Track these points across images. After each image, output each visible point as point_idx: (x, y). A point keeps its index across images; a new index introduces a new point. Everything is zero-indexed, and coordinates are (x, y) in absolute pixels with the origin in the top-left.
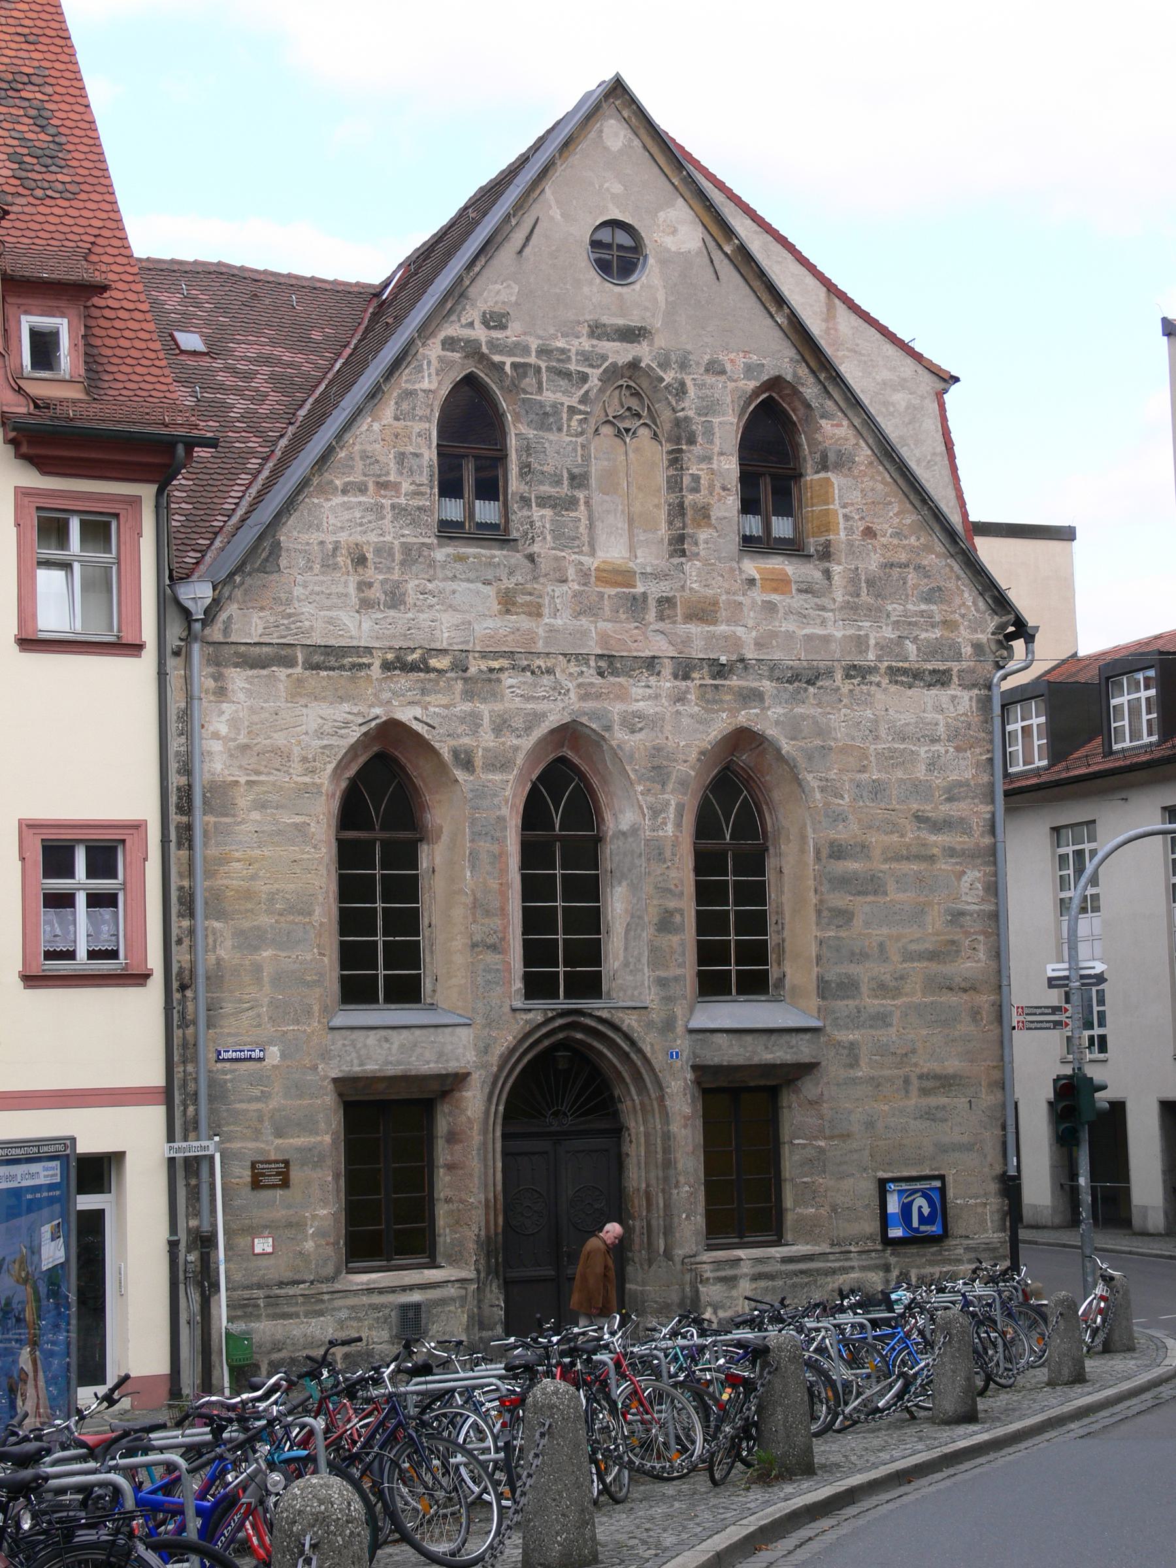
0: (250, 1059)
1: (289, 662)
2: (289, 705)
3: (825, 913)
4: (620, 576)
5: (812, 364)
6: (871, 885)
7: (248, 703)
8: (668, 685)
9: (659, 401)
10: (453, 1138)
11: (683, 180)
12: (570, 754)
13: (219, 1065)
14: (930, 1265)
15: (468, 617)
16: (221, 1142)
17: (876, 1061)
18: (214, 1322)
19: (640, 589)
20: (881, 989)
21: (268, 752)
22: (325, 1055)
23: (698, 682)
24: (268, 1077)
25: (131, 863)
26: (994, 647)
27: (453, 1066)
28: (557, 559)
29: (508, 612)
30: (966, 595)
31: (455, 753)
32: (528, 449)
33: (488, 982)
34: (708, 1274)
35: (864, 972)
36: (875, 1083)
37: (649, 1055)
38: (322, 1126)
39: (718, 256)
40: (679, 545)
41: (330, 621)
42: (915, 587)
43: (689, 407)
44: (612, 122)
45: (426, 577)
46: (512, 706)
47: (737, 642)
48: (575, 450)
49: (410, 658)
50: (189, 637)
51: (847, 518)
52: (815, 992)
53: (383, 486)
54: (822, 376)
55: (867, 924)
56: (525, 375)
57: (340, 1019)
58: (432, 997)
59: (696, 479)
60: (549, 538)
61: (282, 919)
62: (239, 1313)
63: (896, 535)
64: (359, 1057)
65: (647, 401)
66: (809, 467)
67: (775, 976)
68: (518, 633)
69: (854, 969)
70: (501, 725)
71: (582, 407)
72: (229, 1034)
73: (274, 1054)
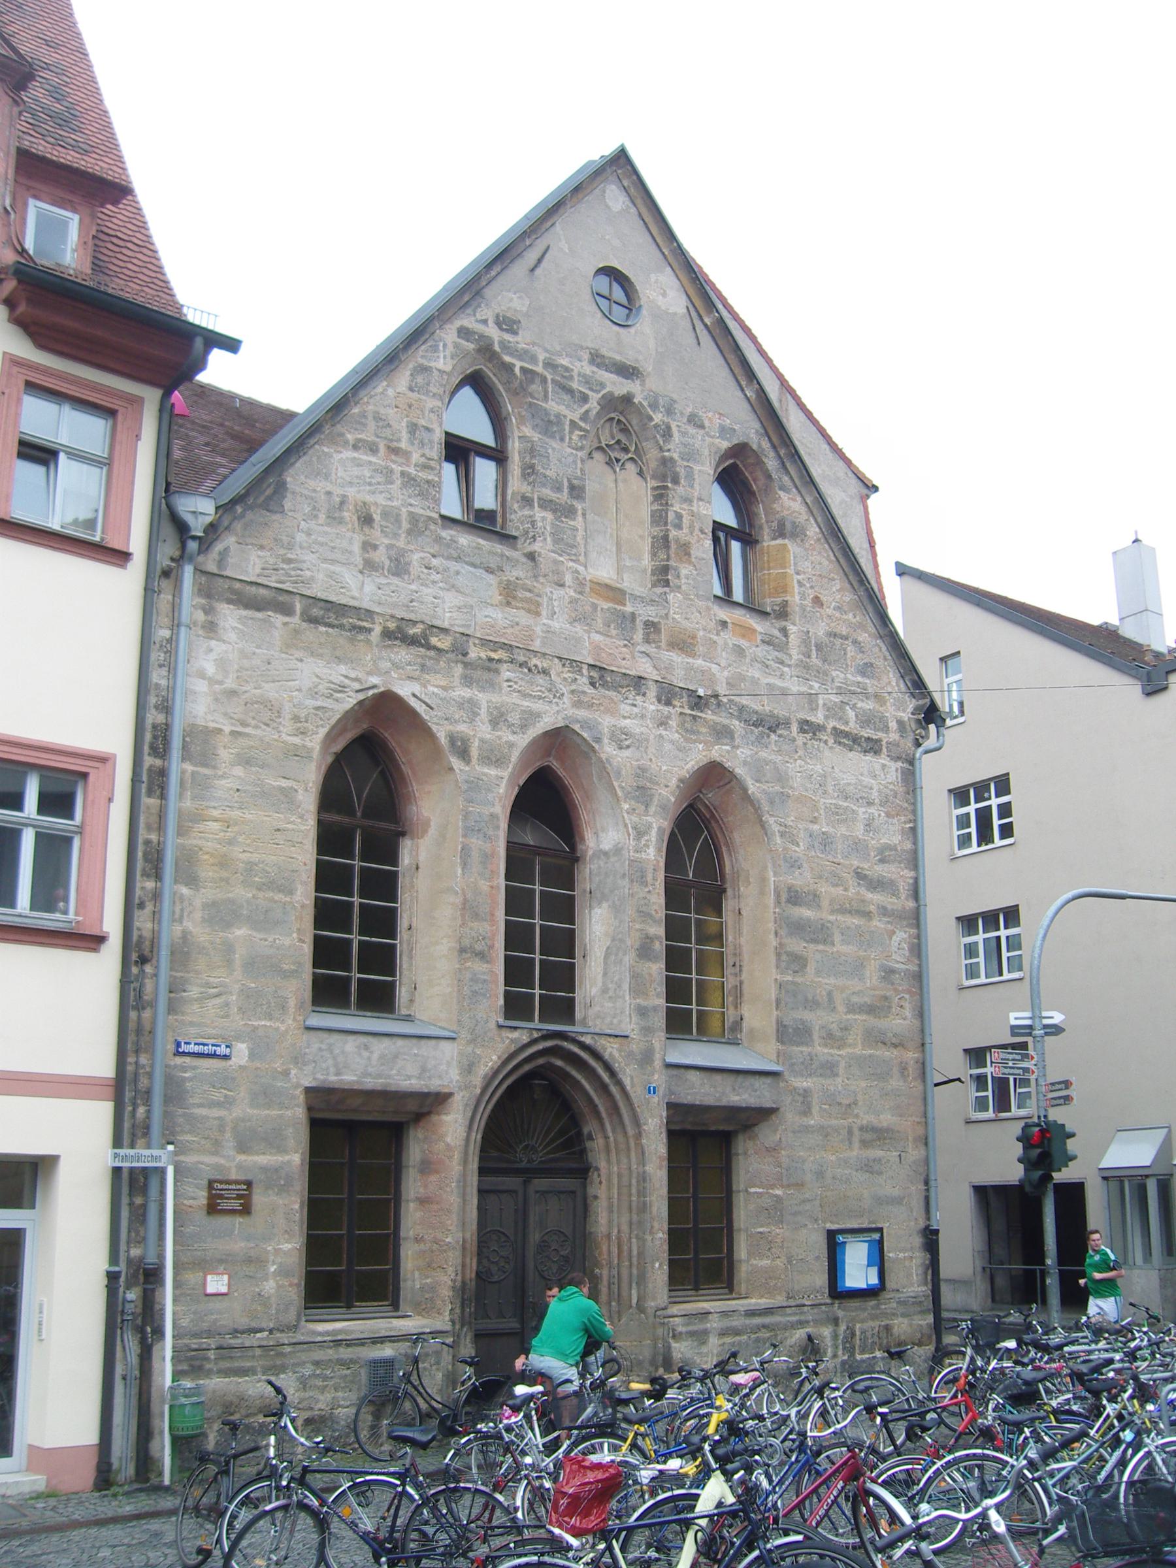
0: (214, 1055)
1: (287, 610)
2: (283, 655)
3: (784, 957)
4: (615, 593)
5: (775, 439)
6: (819, 934)
7: (240, 645)
8: (652, 707)
9: (647, 440)
10: (427, 1167)
11: (672, 251)
12: (556, 765)
13: (179, 1060)
14: (872, 1319)
15: (471, 601)
16: (175, 1153)
17: (825, 1110)
18: (156, 1379)
19: (629, 608)
20: (830, 1038)
21: (257, 702)
22: (298, 1059)
23: (679, 710)
24: (234, 1079)
25: (93, 802)
26: (914, 726)
27: (434, 1084)
28: (555, 562)
29: (508, 604)
30: (891, 675)
31: (452, 739)
32: (532, 451)
33: (475, 993)
34: (680, 1329)
35: (817, 1019)
36: (825, 1132)
37: (628, 1088)
38: (291, 1143)
39: (699, 327)
40: (662, 575)
41: (331, 575)
42: (853, 659)
43: (674, 450)
44: (613, 187)
45: (432, 551)
46: (509, 700)
47: (712, 680)
48: (575, 462)
49: (412, 631)
50: (181, 558)
51: (800, 583)
52: (775, 1037)
53: (396, 451)
54: (782, 452)
55: (818, 972)
56: (532, 382)
57: (316, 1020)
58: (408, 1008)
59: (679, 517)
60: (549, 539)
61: (261, 894)
62: (185, 1367)
63: (838, 608)
64: (336, 1065)
65: (635, 438)
66: (766, 534)
67: (731, 1020)
68: (517, 628)
69: (807, 1016)
70: (497, 719)
71: (582, 424)
72: (192, 1024)
73: (241, 1052)
